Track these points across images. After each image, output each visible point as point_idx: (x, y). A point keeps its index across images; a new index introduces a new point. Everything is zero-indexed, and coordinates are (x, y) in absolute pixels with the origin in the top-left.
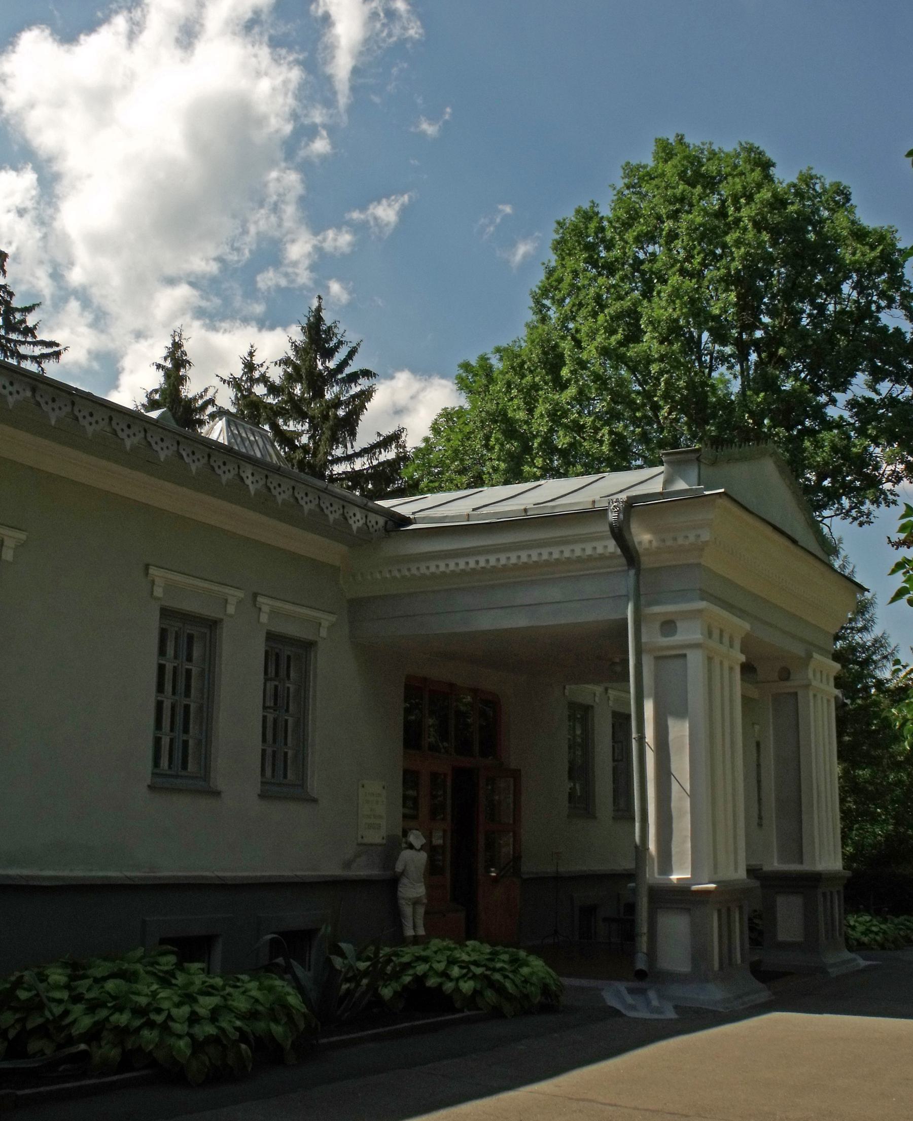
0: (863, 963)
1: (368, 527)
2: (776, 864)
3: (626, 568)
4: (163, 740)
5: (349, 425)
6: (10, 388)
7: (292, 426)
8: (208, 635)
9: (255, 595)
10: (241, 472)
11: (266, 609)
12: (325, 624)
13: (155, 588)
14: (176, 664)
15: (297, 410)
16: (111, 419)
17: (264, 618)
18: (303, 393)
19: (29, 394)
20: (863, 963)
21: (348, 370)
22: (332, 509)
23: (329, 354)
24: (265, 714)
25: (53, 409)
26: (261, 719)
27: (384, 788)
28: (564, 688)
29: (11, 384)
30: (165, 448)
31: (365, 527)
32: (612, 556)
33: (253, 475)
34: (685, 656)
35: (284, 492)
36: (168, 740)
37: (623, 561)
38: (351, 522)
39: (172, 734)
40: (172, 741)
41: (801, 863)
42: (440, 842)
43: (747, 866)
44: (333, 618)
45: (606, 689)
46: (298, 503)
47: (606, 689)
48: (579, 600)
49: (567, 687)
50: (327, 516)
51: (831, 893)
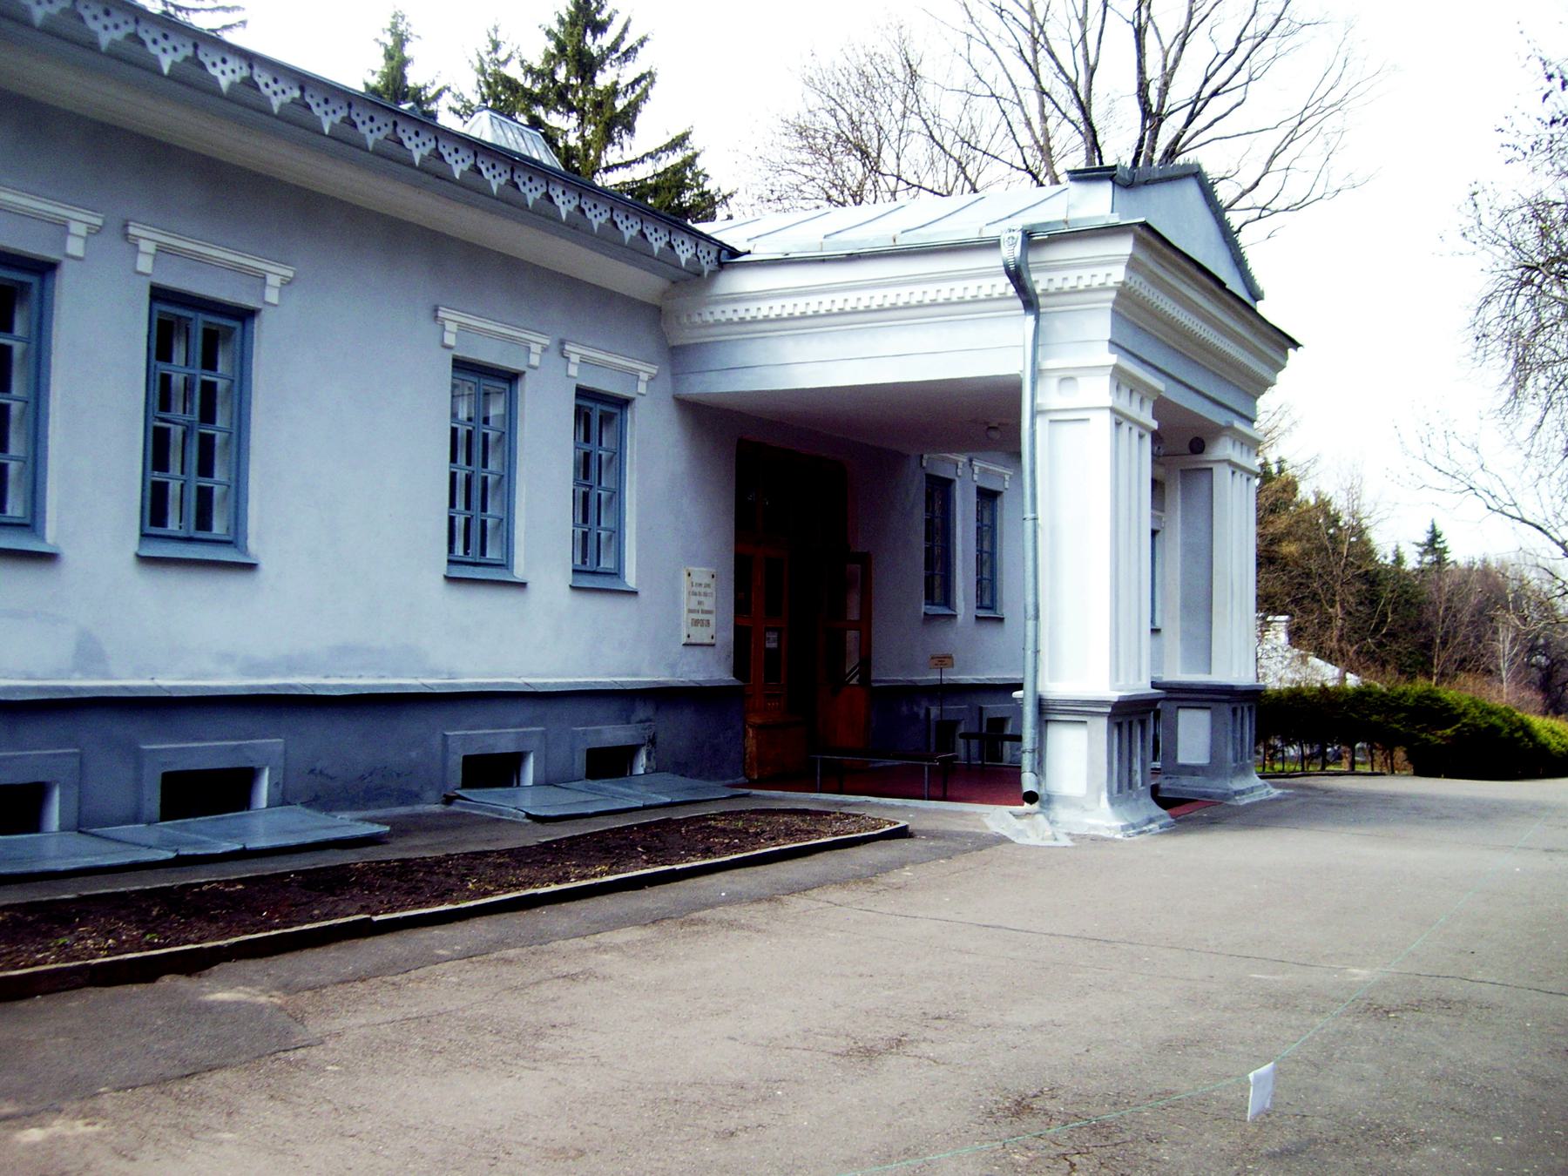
0: (1276, 793)
1: (698, 258)
2: (1179, 674)
3: (1023, 311)
4: (457, 519)
5: (626, 121)
6: (274, 87)
7: (554, 120)
8: (508, 390)
9: (562, 343)
10: (550, 190)
11: (575, 358)
12: (644, 377)
13: (446, 334)
14: (470, 428)
15: (560, 98)
16: (395, 124)
17: (573, 371)
18: (567, 79)
19: (297, 94)
20: (1276, 793)
21: (623, 47)
22: (658, 236)
23: (600, 28)
24: (455, 425)
25: (326, 113)
26: (449, 433)
27: (713, 576)
28: (922, 456)
29: (276, 81)
30: (421, 145)
31: (696, 259)
32: (1003, 297)
33: (564, 193)
34: (1211, 469)
35: (601, 214)
36: (463, 521)
37: (1019, 303)
38: (678, 251)
39: (468, 512)
40: (468, 521)
41: (1210, 673)
42: (774, 645)
43: (1152, 677)
44: (653, 370)
45: (971, 460)
46: (617, 228)
47: (971, 460)
48: (444, 179)
49: (926, 456)
50: (622, 232)
51: (1242, 708)
